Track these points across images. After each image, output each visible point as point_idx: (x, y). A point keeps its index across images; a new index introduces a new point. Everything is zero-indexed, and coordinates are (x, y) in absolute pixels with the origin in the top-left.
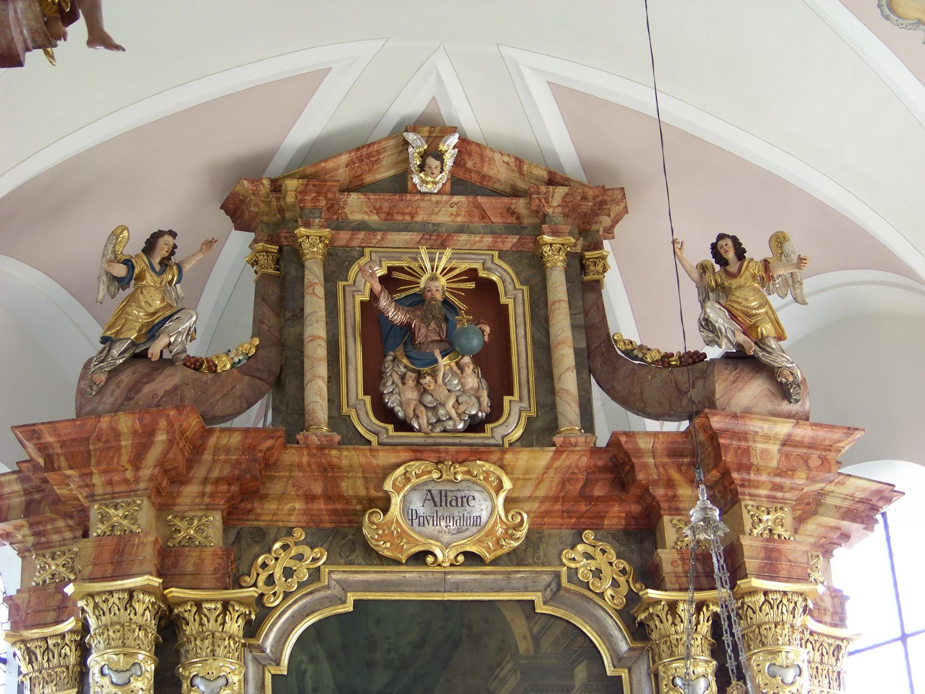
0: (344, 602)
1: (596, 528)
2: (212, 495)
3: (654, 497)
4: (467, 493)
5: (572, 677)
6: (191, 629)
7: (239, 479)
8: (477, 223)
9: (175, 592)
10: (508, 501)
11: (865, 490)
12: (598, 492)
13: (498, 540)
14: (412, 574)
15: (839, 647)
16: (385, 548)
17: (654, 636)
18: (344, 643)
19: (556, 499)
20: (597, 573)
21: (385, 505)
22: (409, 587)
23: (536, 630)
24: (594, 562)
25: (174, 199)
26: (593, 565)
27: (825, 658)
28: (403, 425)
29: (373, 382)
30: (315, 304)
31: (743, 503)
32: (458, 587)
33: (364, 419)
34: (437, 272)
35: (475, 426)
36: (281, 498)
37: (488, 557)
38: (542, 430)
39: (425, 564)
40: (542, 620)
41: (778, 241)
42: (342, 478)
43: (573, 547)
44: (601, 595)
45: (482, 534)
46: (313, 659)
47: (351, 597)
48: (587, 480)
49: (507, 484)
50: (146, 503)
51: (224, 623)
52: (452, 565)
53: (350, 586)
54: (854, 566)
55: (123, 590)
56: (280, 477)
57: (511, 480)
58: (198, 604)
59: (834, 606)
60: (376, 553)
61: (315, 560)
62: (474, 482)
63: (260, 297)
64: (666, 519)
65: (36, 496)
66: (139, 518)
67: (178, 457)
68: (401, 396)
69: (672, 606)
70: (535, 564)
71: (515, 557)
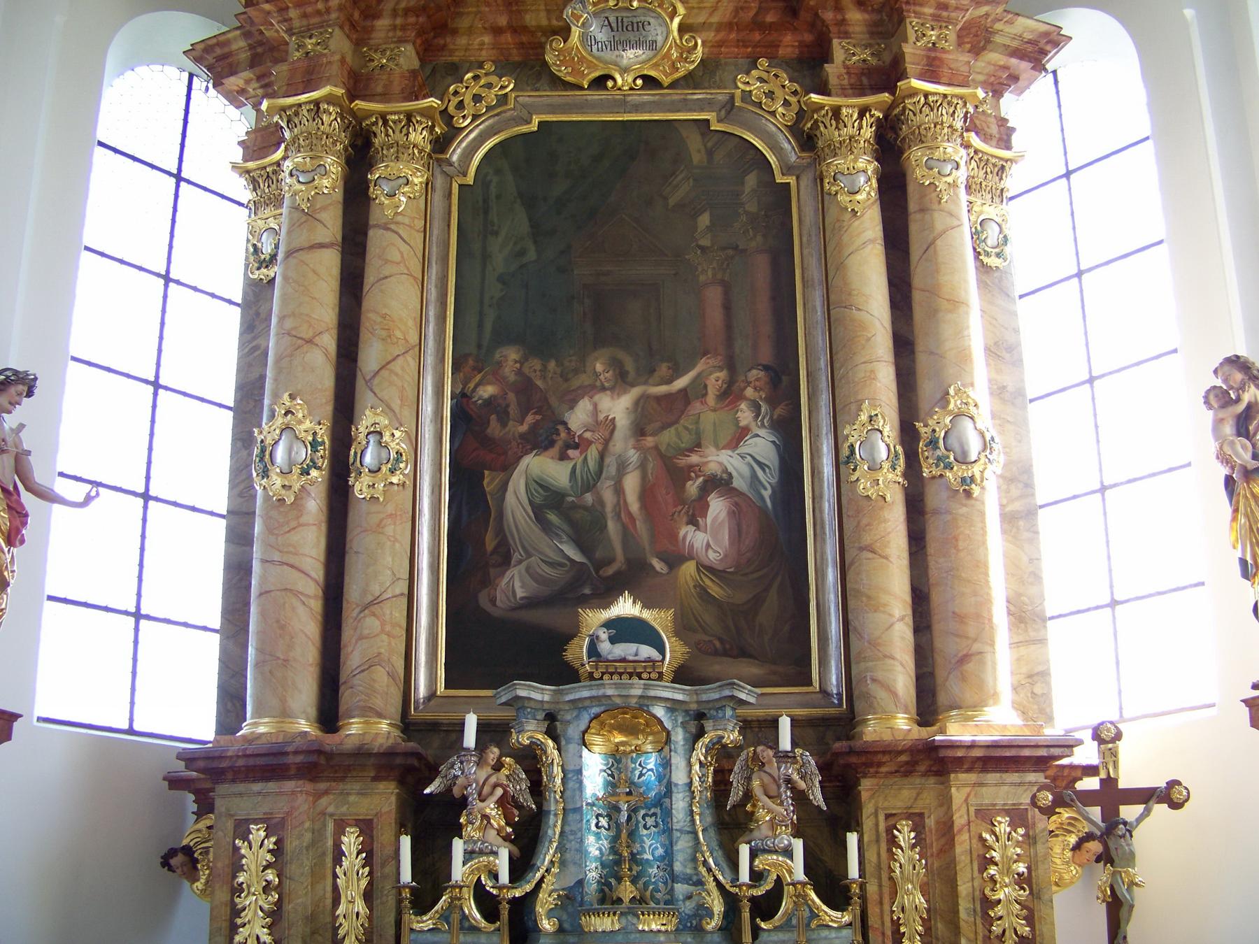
0: (529, 122)
1: (770, 58)
2: (403, 28)
3: (823, 21)
4: (643, 19)
5: (743, 184)
7: (424, 9)
9: (360, 104)
10: (682, 29)
11: (1032, 31)
12: (770, 18)
13: (673, 63)
14: (596, 95)
15: (1003, 167)
16: (563, 72)
17: (820, 144)
18: (523, 158)
19: (729, 26)
21: (565, 32)
22: (595, 112)
23: (710, 144)
26: (766, 88)
27: (990, 176)
31: (908, 21)
36: (470, 31)
37: (666, 81)
39: (606, 88)
40: (716, 137)
42: (526, 11)
43: (748, 73)
44: (773, 113)
45: (659, 57)
46: (498, 172)
47: (536, 120)
48: (760, 8)
49: (681, 10)
50: (337, 31)
51: (407, 134)
52: (631, 89)
53: (538, 112)
54: (1024, 108)
55: (310, 102)
56: (469, 13)
57: (686, 8)
58: (383, 117)
59: (999, 132)
60: (559, 78)
61: (503, 88)
62: (649, 9)
64: (835, 42)
65: (259, 50)
69: (836, 112)
70: (710, 88)
71: (690, 80)
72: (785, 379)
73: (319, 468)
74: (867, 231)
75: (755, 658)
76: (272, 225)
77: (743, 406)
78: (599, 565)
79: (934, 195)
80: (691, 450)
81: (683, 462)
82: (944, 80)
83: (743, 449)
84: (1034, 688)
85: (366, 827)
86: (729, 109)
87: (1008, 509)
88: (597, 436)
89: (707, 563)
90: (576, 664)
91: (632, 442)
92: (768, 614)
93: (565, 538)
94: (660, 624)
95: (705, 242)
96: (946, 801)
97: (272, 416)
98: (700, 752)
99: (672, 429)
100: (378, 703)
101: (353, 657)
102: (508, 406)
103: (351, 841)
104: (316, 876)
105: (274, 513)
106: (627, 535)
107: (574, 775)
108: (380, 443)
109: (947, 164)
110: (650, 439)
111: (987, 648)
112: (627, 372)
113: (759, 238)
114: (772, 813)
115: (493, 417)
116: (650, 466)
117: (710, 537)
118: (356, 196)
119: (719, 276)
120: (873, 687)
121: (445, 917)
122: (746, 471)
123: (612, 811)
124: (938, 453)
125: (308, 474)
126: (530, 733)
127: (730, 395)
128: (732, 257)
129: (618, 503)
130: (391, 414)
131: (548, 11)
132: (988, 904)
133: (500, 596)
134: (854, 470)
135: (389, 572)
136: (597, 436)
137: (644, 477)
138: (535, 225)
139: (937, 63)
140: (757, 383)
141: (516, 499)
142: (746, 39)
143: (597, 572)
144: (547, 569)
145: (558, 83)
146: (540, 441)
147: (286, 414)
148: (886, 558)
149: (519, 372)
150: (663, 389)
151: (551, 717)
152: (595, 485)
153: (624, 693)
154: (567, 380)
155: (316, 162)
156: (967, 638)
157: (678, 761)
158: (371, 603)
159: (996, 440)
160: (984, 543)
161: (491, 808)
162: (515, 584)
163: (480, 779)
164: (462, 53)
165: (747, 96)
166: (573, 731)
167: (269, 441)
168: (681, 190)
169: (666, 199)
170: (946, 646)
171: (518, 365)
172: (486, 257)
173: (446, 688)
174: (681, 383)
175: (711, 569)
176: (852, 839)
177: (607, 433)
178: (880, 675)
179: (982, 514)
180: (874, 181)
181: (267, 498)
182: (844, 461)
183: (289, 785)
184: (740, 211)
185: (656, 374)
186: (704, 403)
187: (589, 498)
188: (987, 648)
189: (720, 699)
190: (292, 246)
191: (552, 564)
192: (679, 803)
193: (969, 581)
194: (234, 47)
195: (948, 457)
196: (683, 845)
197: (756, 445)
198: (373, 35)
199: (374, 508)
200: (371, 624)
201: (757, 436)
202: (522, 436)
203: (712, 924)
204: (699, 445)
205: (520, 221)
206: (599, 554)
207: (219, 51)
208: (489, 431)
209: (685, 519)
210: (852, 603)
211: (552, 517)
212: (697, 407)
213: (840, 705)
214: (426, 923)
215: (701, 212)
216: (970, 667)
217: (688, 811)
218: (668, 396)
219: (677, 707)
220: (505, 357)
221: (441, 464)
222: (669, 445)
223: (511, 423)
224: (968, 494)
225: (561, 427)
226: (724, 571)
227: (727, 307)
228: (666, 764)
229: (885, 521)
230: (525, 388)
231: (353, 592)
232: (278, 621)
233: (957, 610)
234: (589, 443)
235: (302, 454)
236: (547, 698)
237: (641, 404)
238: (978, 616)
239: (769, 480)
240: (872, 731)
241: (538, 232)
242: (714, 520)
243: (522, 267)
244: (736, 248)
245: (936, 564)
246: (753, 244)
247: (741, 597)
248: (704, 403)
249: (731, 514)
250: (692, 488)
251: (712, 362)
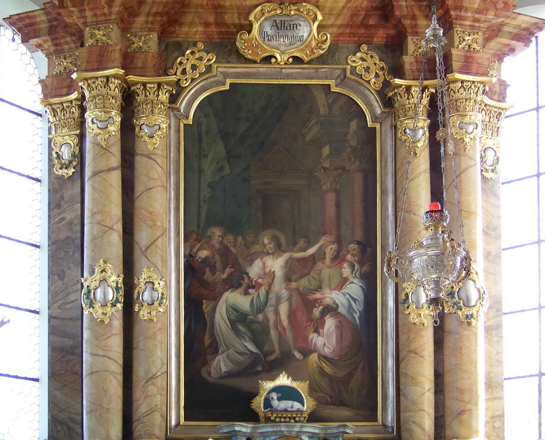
1: (368, 43)
2: (152, 23)
3: (404, 25)
4: (296, 22)
5: (349, 127)
6: (140, 98)
9: (131, 78)
12: (371, 22)
13: (312, 49)
14: (263, 68)
17: (396, 105)
19: (347, 26)
20: (367, 69)
22: (260, 76)
24: (366, 64)
26: (365, 64)
27: (492, 120)
31: (455, 29)
32: (288, 76)
36: (191, 24)
37: (306, 59)
39: (271, 63)
42: (226, 13)
43: (354, 54)
44: (369, 82)
45: (304, 46)
46: (206, 116)
47: (228, 82)
49: (320, 17)
51: (158, 95)
52: (285, 64)
55: (103, 77)
56: (191, 12)
57: (322, 14)
58: (144, 84)
60: (243, 56)
62: (301, 16)
64: (410, 38)
65: (55, 23)
66: (109, 35)
69: (408, 89)
71: (321, 60)
72: (369, 250)
73: (120, 302)
74: (422, 163)
75: (348, 406)
76: (68, 141)
77: (345, 265)
78: (266, 355)
79: (462, 145)
80: (316, 291)
81: (311, 297)
82: (474, 71)
83: (345, 290)
86: (343, 80)
87: (487, 324)
88: (265, 281)
89: (324, 354)
90: (257, 410)
91: (284, 285)
92: (355, 383)
93: (248, 339)
94: (302, 389)
95: (326, 165)
97: (92, 272)
99: (306, 278)
101: (141, 407)
102: (215, 263)
105: (98, 328)
106: (281, 337)
108: (153, 289)
110: (294, 283)
111: (474, 407)
112: (282, 244)
113: (357, 163)
115: (208, 269)
116: (294, 299)
117: (326, 340)
118: (128, 130)
119: (334, 186)
120: (413, 426)
122: (346, 303)
124: (454, 300)
125: (115, 306)
127: (338, 259)
128: (341, 175)
129: (276, 320)
130: (157, 271)
131: (239, 14)
133: (213, 371)
134: (408, 308)
135: (159, 361)
136: (265, 281)
137: (290, 306)
138: (228, 152)
139: (471, 60)
140: (353, 252)
141: (221, 317)
142: (355, 32)
143: (265, 358)
144: (239, 357)
145: (242, 59)
147: (102, 272)
148: (423, 357)
149: (221, 243)
150: (301, 255)
152: (263, 310)
153: (291, 430)
154: (248, 248)
155: (108, 116)
156: (464, 401)
158: (152, 378)
159: (486, 293)
160: (476, 351)
162: (221, 365)
164: (184, 36)
165: (353, 69)
167: (92, 287)
168: (313, 131)
169: (304, 136)
170: (451, 405)
171: (220, 239)
172: (201, 171)
173: (185, 421)
174: (311, 251)
175: (326, 358)
177: (270, 280)
178: (417, 420)
179: (476, 334)
180: (427, 133)
181: (92, 318)
182: (401, 302)
184: (347, 145)
185: (298, 246)
186: (324, 263)
187: (260, 317)
188: (474, 407)
189: (337, 433)
190: (96, 169)
191: (241, 354)
193: (467, 371)
194: (38, 19)
195: (460, 303)
197: (352, 288)
198: (134, 26)
199: (151, 325)
200: (152, 389)
201: (353, 283)
202: (224, 281)
204: (320, 288)
206: (266, 348)
207: (27, 21)
208: (205, 277)
209: (312, 330)
210: (402, 380)
211: (241, 327)
212: (320, 265)
213: (393, 433)
215: (323, 146)
216: (464, 417)
218: (304, 259)
219: (314, 436)
220: (213, 233)
221: (179, 296)
222: (304, 287)
223: (217, 273)
224: (469, 324)
225: (245, 276)
226: (332, 359)
227: (338, 206)
229: (423, 337)
230: (225, 252)
231: (140, 371)
232: (103, 388)
233: (459, 387)
234: (261, 285)
235: (111, 295)
236: (249, 431)
237: (289, 265)
238: (470, 390)
239: (358, 308)
241: (231, 156)
242: (328, 330)
243: (222, 178)
244: (344, 169)
245: (449, 361)
246: (354, 167)
247: (341, 373)
248: (324, 263)
249: (337, 327)
250: (317, 312)
251: (328, 239)
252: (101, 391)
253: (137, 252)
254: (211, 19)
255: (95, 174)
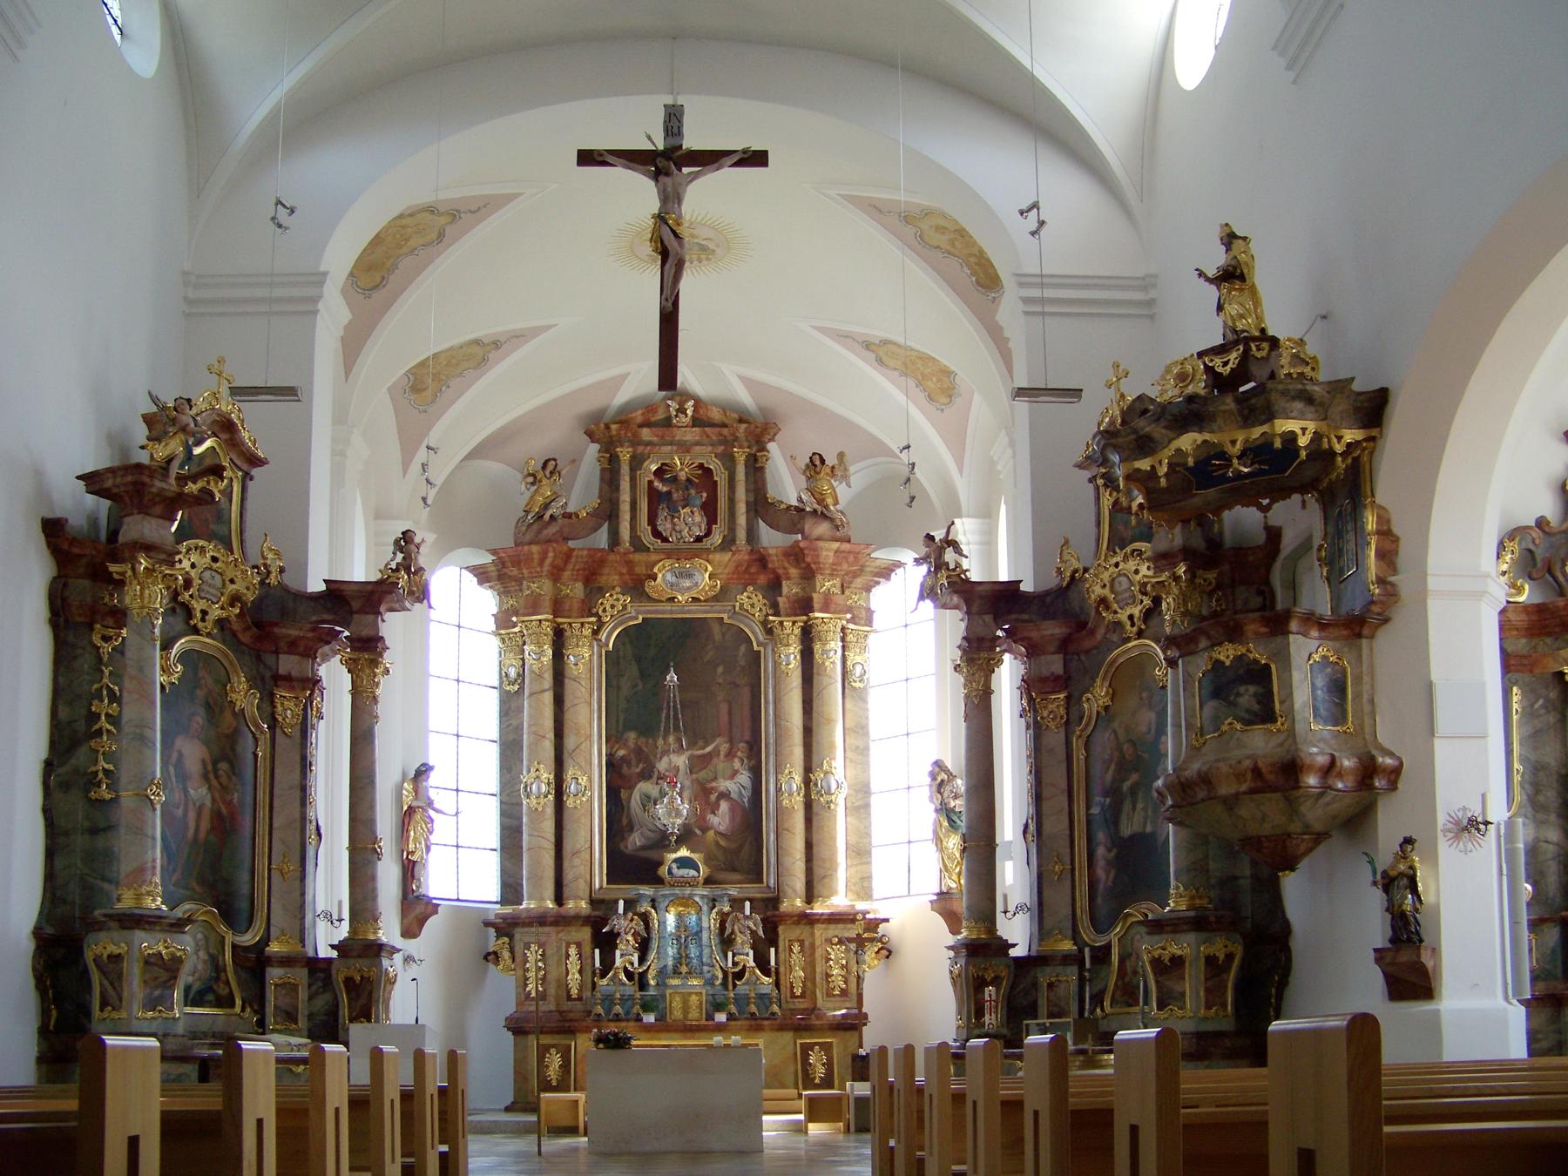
6: (568, 634)
8: (705, 440)
9: (560, 620)
14: (668, 606)
16: (655, 596)
20: (753, 606)
22: (664, 612)
24: (751, 600)
25: (557, 436)
28: (665, 540)
29: (652, 521)
30: (625, 484)
32: (689, 612)
33: (647, 538)
34: (681, 465)
35: (699, 539)
38: (728, 543)
41: (841, 456)
63: (602, 479)
66: (545, 587)
67: (559, 562)
68: (664, 526)
69: (781, 623)
71: (716, 598)
84: (863, 888)
85: (579, 945)
92: (745, 853)
96: (813, 935)
98: (713, 915)
100: (581, 893)
101: (569, 875)
103: (573, 951)
104: (559, 962)
107: (662, 923)
109: (830, 653)
114: (743, 942)
117: (721, 819)
118: (558, 656)
121: (612, 979)
123: (678, 938)
126: (645, 907)
127: (730, 755)
132: (828, 976)
146: (646, 775)
151: (653, 901)
157: (704, 918)
161: (630, 938)
162: (635, 840)
163: (622, 923)
165: (741, 605)
166: (663, 906)
170: (817, 871)
172: (619, 688)
174: (708, 749)
176: (773, 950)
181: (529, 807)
183: (547, 929)
192: (705, 935)
196: (706, 951)
200: (577, 861)
203: (718, 982)
205: (634, 670)
212: (715, 760)
214: (605, 982)
217: (709, 937)
218: (703, 756)
227: (730, 713)
228: (700, 919)
230: (638, 751)
231: (568, 847)
235: (544, 788)
239: (747, 794)
240: (785, 906)
241: (643, 675)
247: (733, 846)
250: (713, 797)
252: (536, 862)
253: (566, 755)
254: (624, 570)
255: (531, 695)
